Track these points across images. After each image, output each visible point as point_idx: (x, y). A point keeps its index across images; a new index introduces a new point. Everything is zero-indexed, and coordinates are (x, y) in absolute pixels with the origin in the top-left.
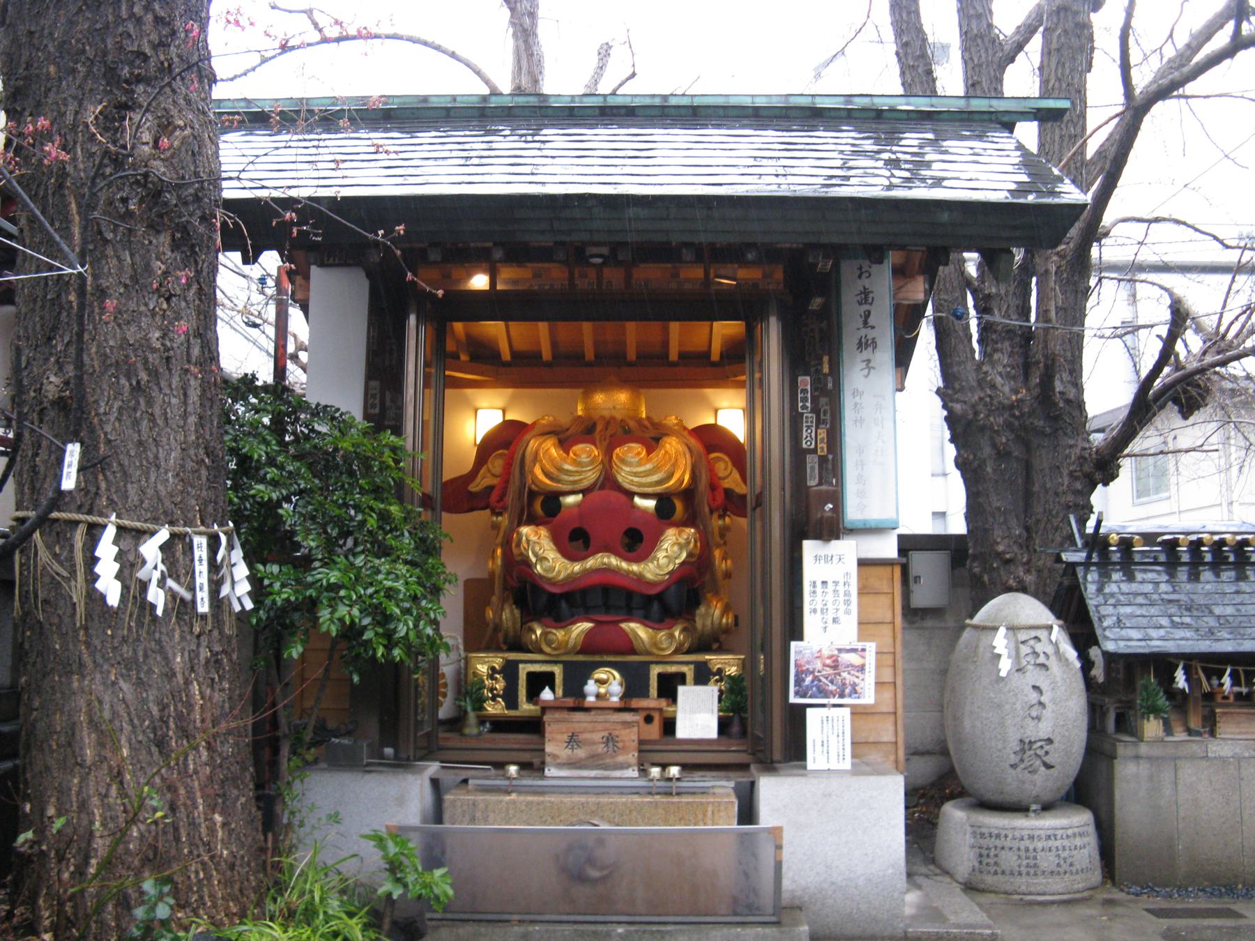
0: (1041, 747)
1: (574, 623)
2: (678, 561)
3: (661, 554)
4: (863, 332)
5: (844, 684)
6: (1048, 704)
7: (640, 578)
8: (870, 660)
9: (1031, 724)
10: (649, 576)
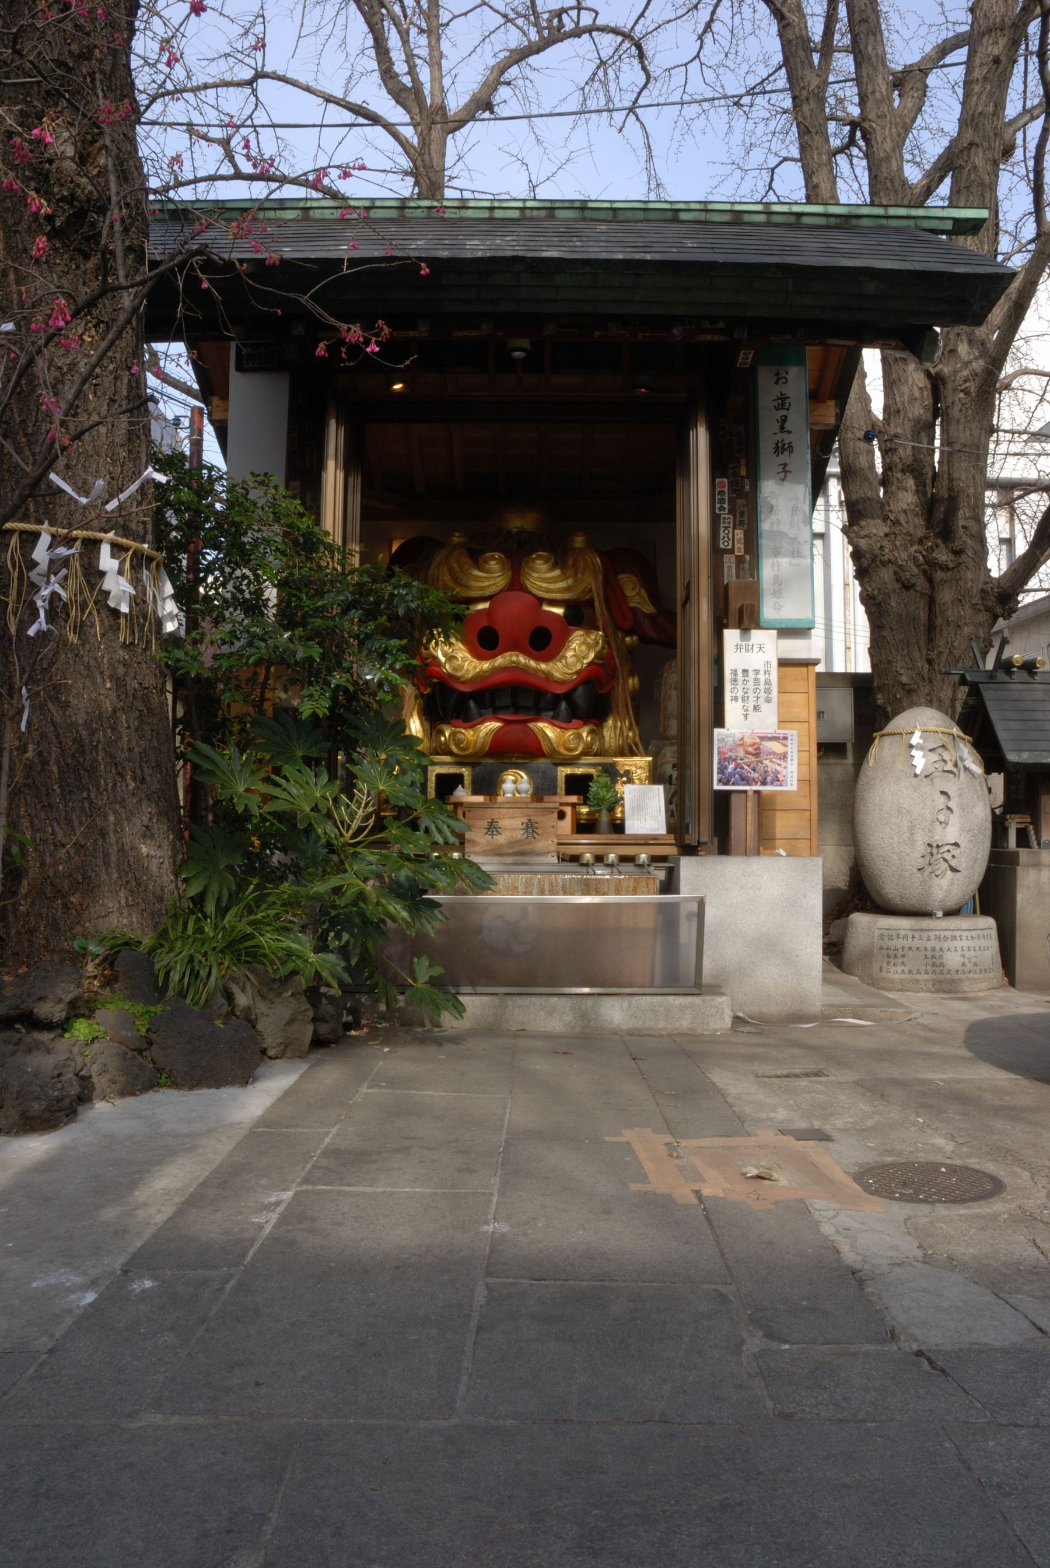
0: (949, 851)
1: (482, 722)
2: (585, 661)
3: (570, 654)
4: (780, 436)
5: (766, 772)
6: (954, 809)
7: (548, 677)
8: (793, 749)
9: (938, 828)
10: (557, 675)
